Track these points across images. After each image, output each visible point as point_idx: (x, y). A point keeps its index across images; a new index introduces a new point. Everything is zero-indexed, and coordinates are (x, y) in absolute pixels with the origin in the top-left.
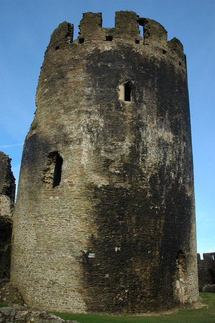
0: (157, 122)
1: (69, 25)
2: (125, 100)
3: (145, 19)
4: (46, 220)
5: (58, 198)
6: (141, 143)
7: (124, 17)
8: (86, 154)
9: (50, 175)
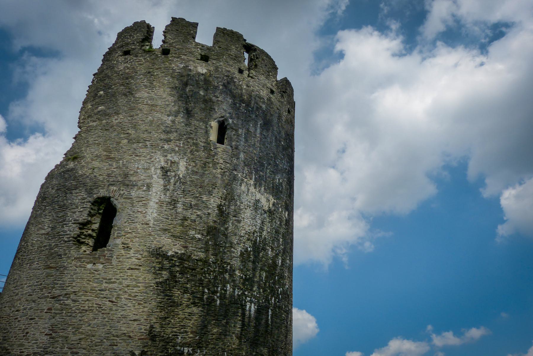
0: (256, 178)
1: (148, 26)
2: (218, 143)
3: (253, 46)
4: (74, 301)
5: (100, 266)
6: (234, 201)
7: (286, 83)
8: (156, 206)
9: (90, 232)
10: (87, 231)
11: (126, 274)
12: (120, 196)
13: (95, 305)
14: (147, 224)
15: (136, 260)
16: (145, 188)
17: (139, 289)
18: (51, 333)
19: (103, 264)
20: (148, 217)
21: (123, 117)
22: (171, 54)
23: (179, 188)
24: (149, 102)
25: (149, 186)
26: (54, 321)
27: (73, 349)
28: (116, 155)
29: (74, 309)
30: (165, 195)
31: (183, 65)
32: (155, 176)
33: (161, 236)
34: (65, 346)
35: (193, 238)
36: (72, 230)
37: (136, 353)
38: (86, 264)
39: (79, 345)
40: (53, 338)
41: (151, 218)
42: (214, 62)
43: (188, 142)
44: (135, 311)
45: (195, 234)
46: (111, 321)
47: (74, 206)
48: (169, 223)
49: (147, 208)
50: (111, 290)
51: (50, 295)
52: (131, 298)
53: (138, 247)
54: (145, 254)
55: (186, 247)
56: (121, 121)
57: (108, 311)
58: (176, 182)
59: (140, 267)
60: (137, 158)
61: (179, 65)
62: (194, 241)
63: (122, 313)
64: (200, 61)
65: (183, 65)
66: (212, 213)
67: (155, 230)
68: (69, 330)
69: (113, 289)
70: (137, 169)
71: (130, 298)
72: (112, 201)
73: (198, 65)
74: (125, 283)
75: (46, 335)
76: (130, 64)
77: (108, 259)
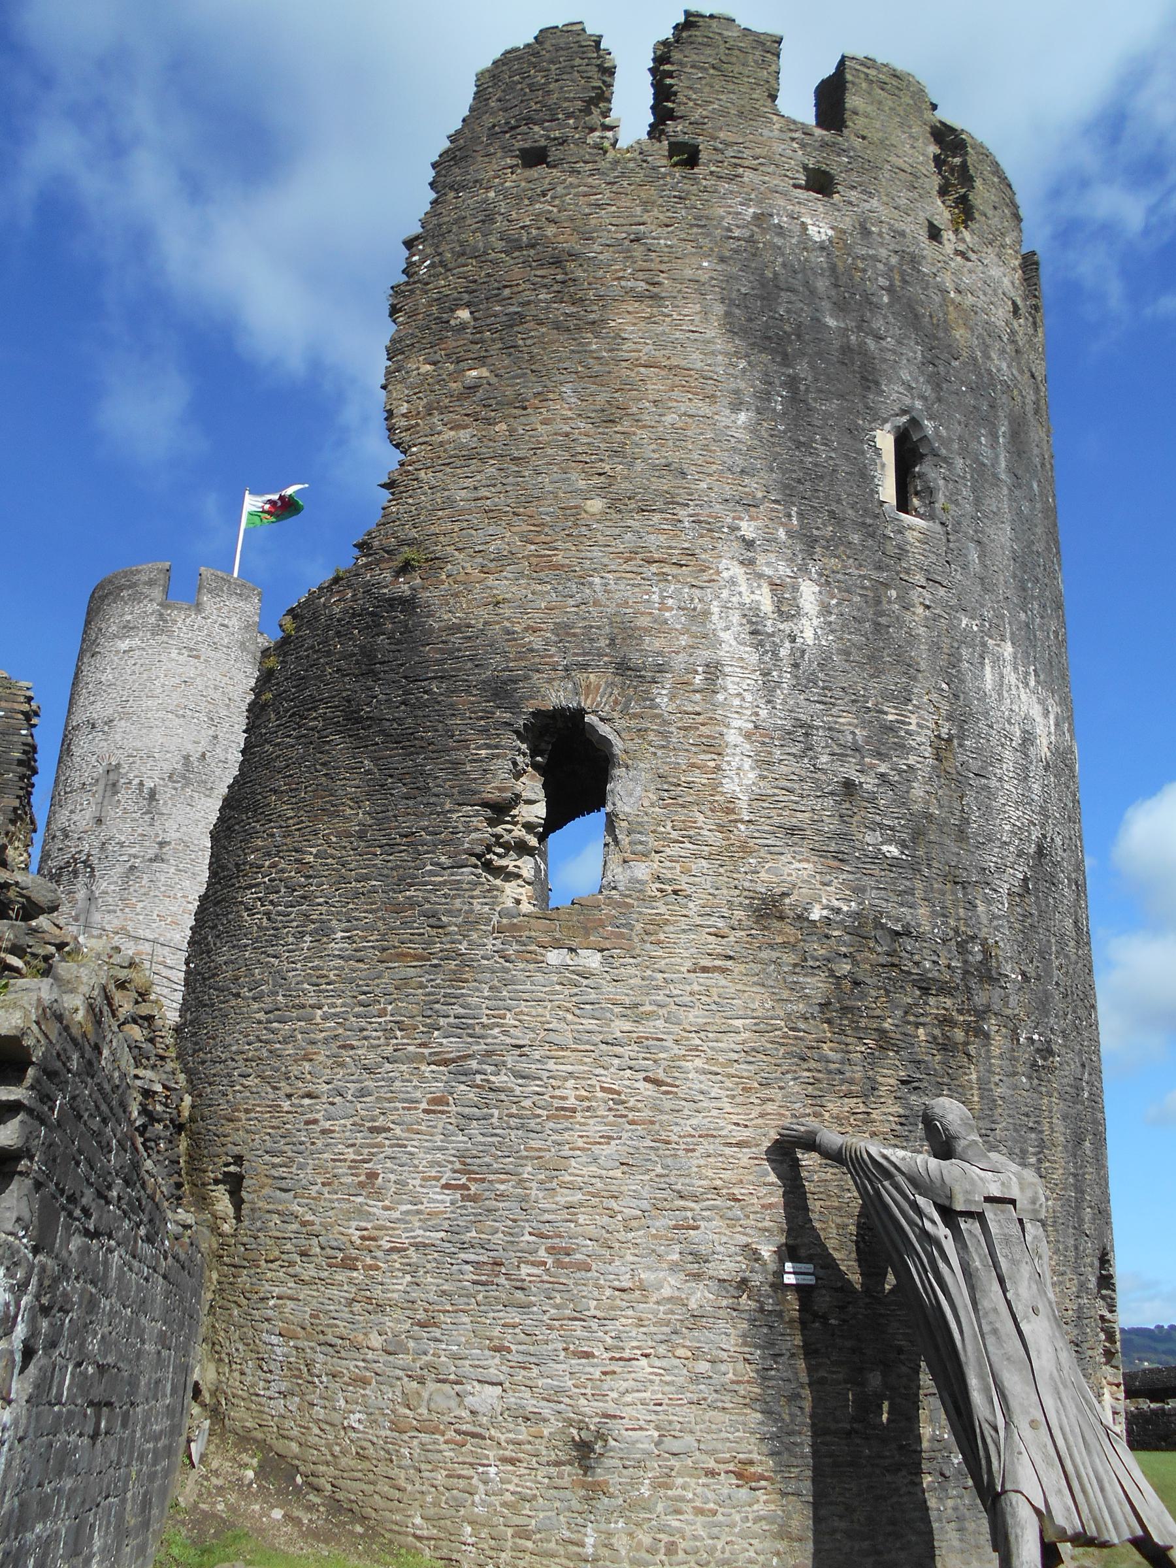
5: (592, 960)
9: (519, 832)
10: (510, 831)
11: (688, 988)
13: (600, 1094)
17: (739, 1038)
22: (704, 164)
23: (809, 681)
25: (714, 670)
29: (527, 1103)
31: (751, 210)
37: (763, 1253)
40: (474, 1199)
41: (738, 789)
42: (853, 195)
44: (738, 1114)
45: (882, 843)
46: (664, 1146)
50: (646, 1043)
51: (426, 1051)
52: (719, 1070)
53: (711, 891)
57: (646, 1114)
59: (730, 963)
61: (740, 208)
63: (694, 1121)
66: (919, 766)
67: (758, 831)
69: (653, 1039)
71: (714, 1069)
76: (557, 202)
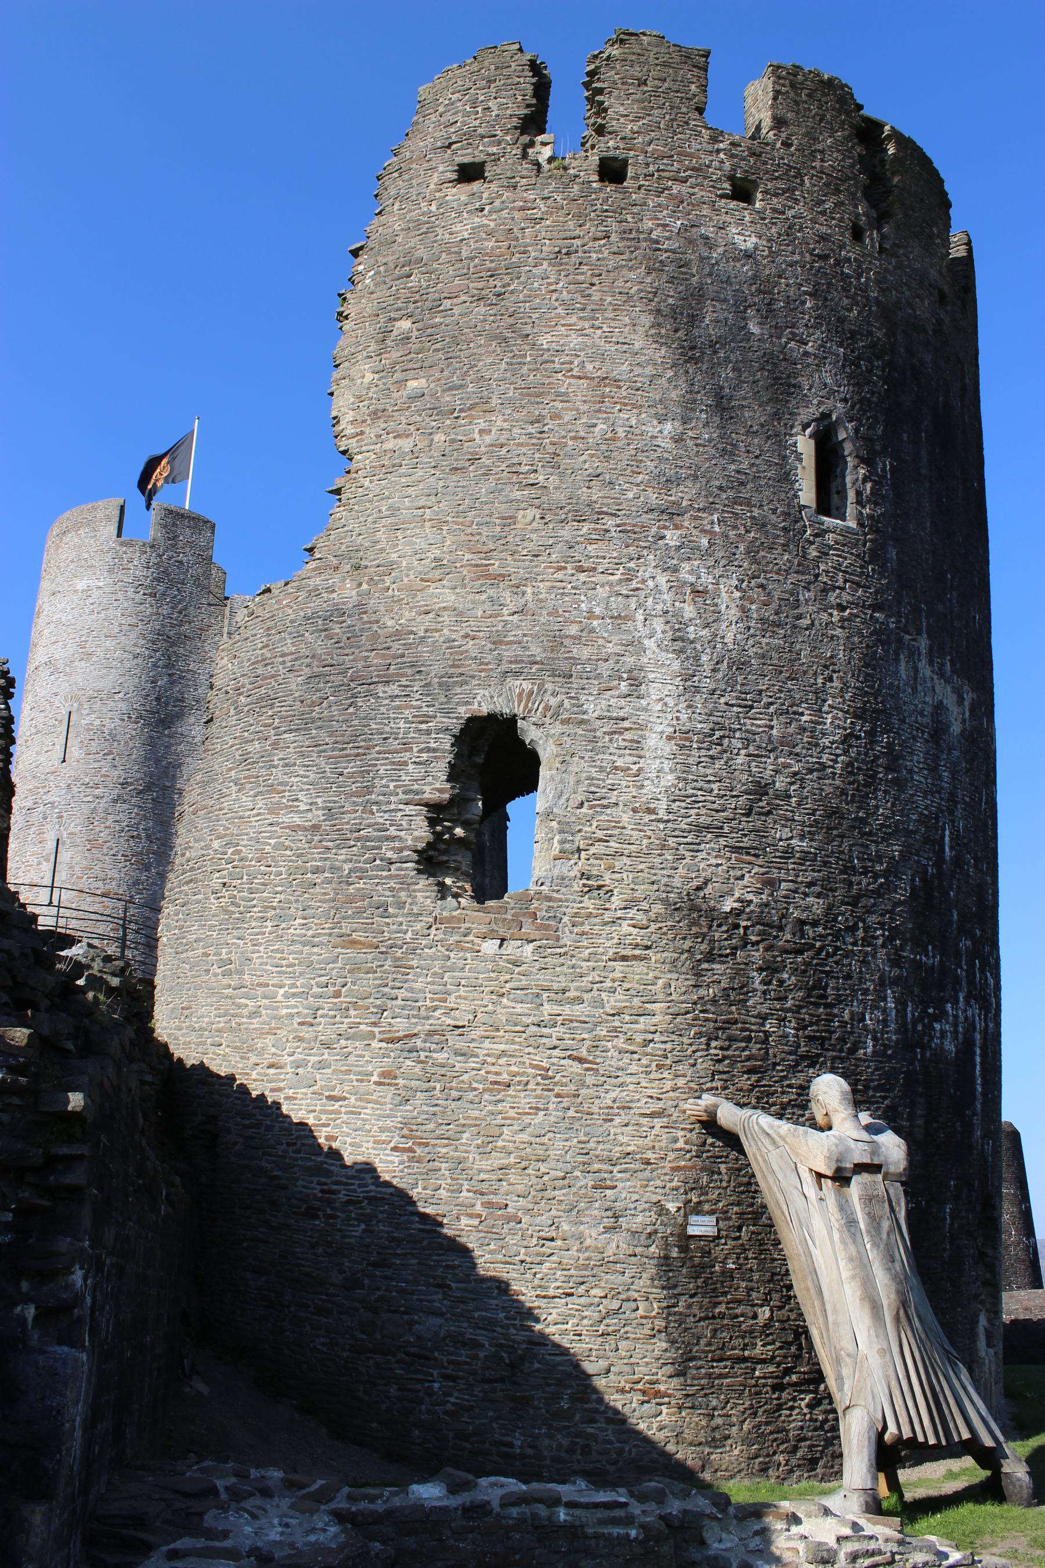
8: (670, 748)
12: (549, 714)
14: (650, 811)
15: (635, 931)
16: (624, 686)
18: (410, 1144)
19: (532, 941)
20: (649, 789)
21: (506, 425)
24: (589, 367)
25: (636, 682)
26: (410, 1111)
27: (487, 1194)
28: (508, 565)
29: (465, 1077)
30: (690, 711)
32: (650, 644)
33: (698, 851)
34: (462, 1185)
35: (787, 852)
36: (404, 823)
38: (477, 941)
39: (505, 1183)
43: (737, 514)
47: (395, 744)
48: (715, 806)
49: (641, 757)
51: (376, 1030)
54: (655, 911)
55: (771, 884)
56: (502, 440)
58: (717, 663)
60: (582, 577)
62: (792, 861)
64: (733, 204)
65: (679, 223)
68: (464, 1141)
69: (577, 1021)
70: (588, 619)
71: (631, 1048)
72: (522, 729)
73: (728, 219)
74: (612, 1003)
75: (395, 1149)
77: (547, 927)
